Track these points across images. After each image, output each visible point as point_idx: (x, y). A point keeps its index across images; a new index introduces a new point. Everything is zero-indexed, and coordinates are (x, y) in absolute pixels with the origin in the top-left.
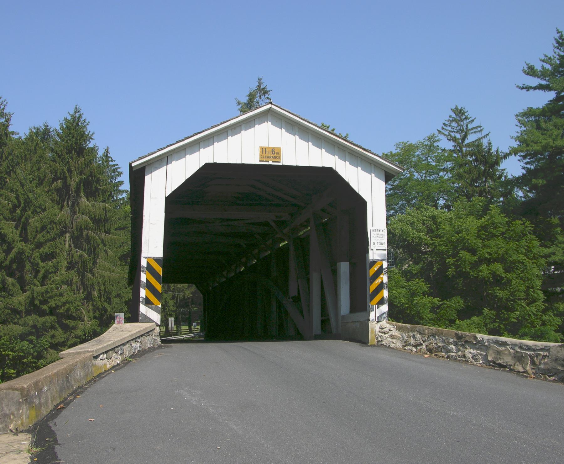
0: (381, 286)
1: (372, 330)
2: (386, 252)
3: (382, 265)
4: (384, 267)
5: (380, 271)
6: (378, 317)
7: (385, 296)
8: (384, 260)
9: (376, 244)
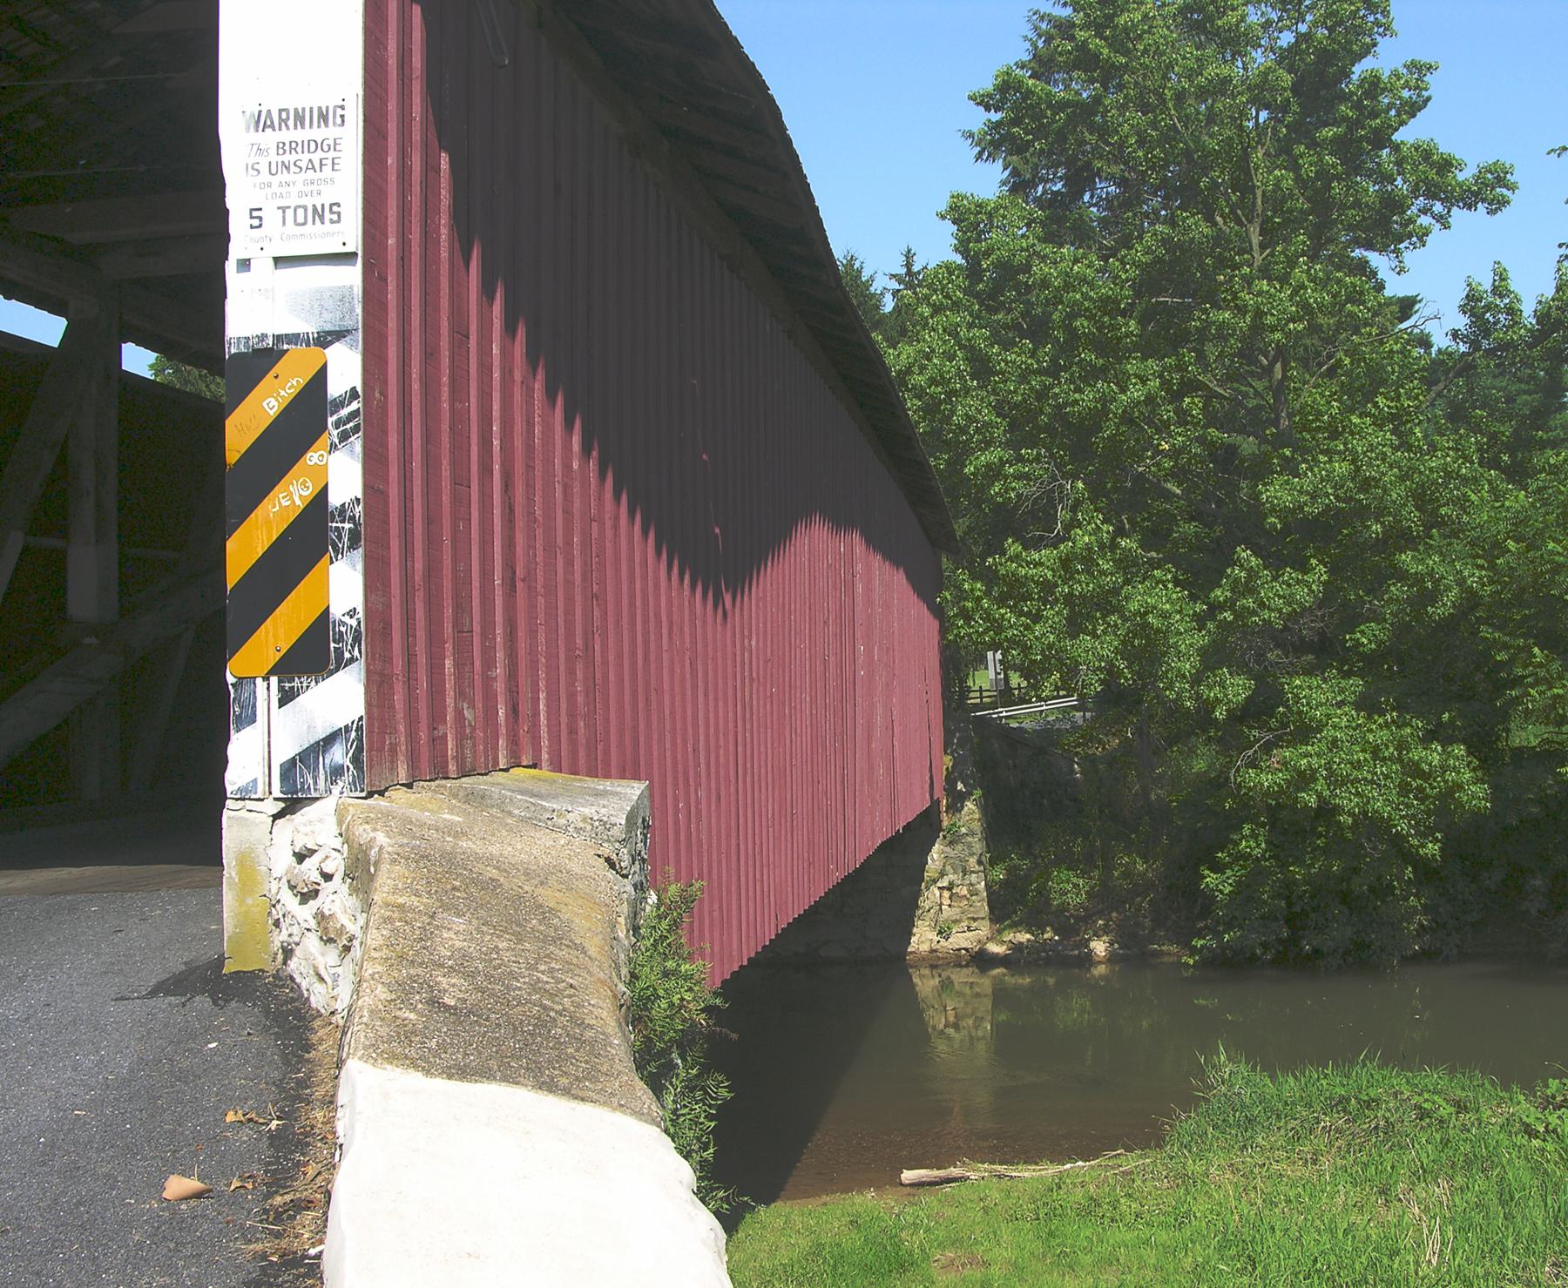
0: (310, 537)
1: (247, 862)
2: (352, 276)
3: (321, 377)
4: (336, 387)
5: (307, 416)
6: (289, 769)
7: (337, 611)
8: (339, 335)
9: (271, 216)
